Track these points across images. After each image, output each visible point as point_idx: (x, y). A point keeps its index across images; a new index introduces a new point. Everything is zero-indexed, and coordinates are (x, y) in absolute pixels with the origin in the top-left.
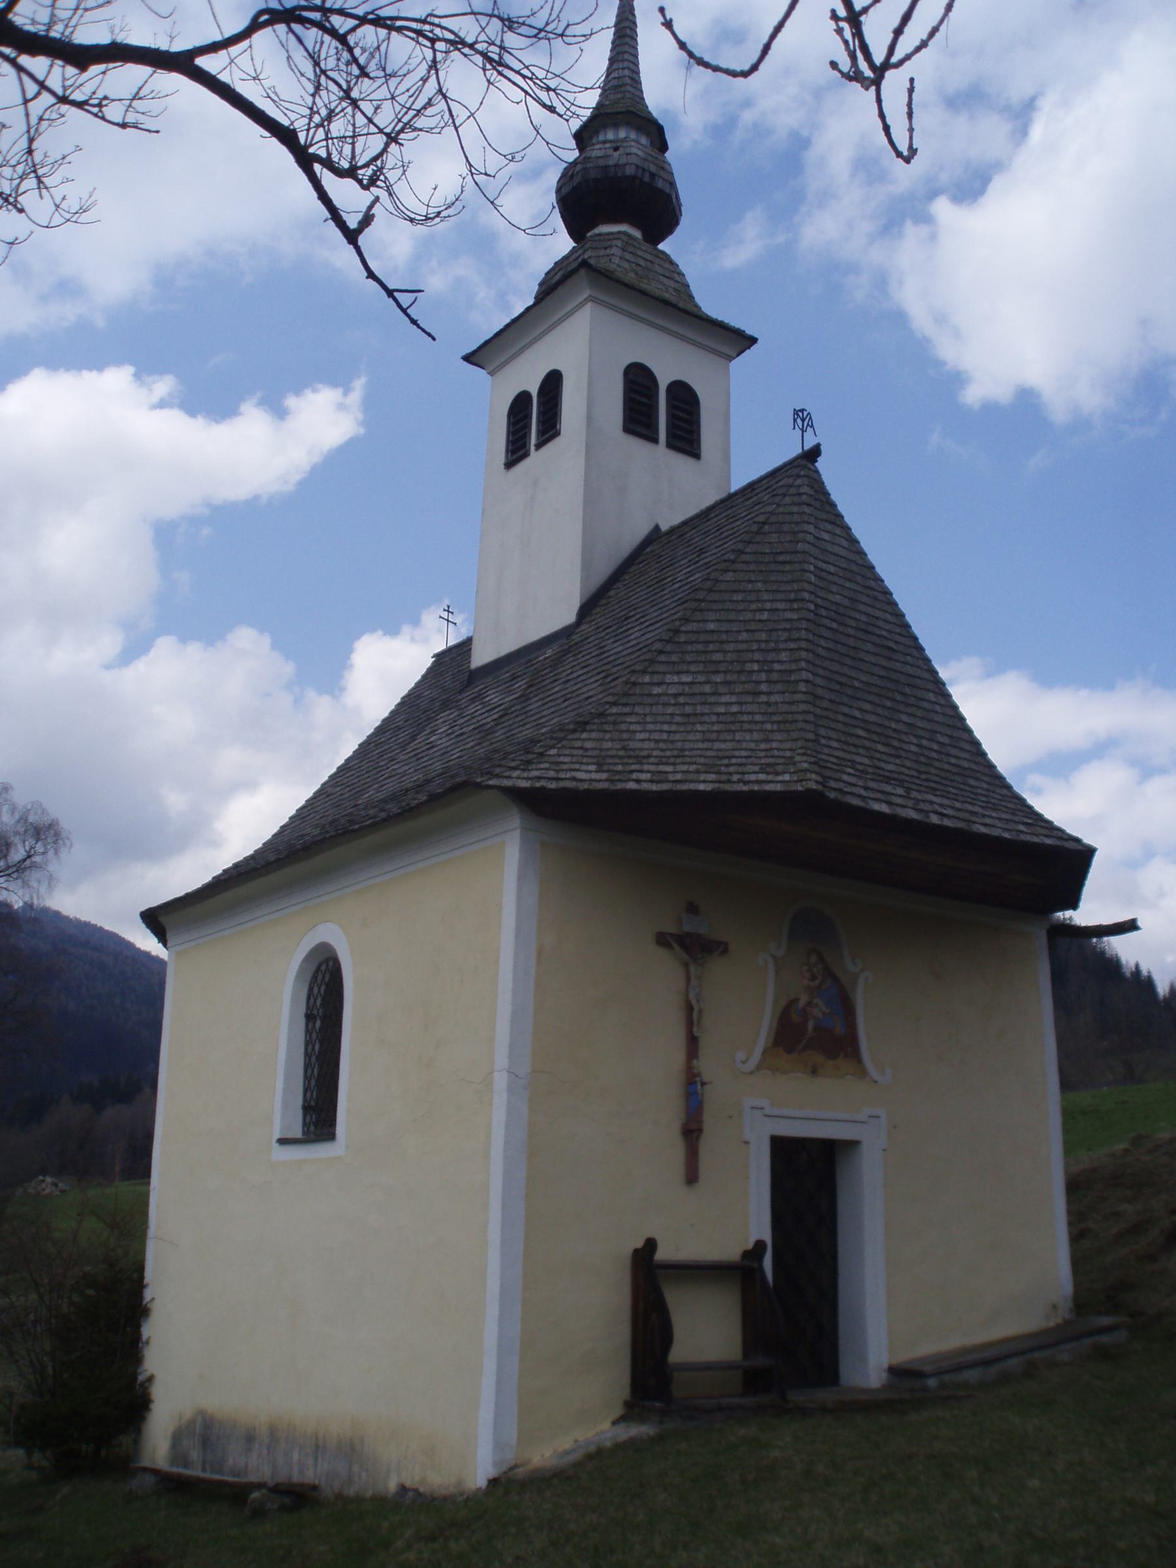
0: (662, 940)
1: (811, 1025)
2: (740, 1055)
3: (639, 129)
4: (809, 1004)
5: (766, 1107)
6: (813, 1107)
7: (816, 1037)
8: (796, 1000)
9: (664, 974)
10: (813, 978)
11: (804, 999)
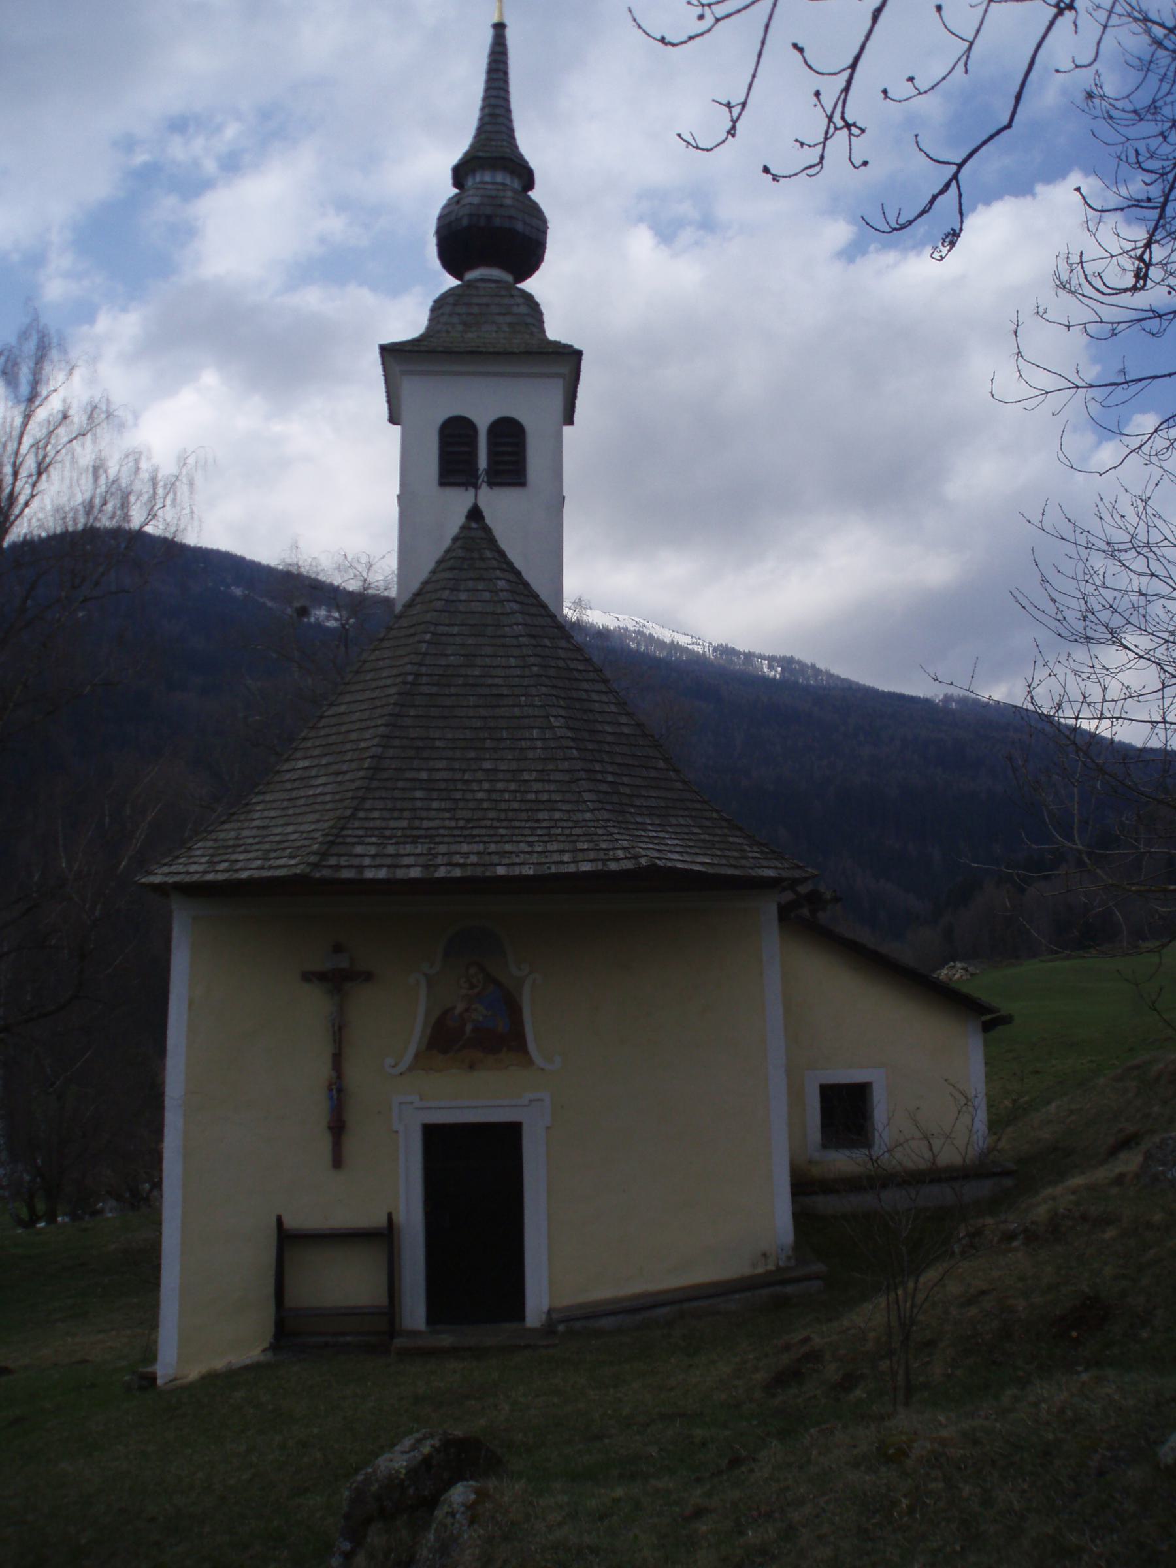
0: (307, 977)
1: (469, 1028)
2: (389, 1061)
3: (512, 173)
4: (467, 1010)
5: (413, 1099)
6: (472, 1097)
7: (481, 1033)
8: (454, 1008)
9: (314, 1005)
10: (472, 986)
11: (460, 1007)
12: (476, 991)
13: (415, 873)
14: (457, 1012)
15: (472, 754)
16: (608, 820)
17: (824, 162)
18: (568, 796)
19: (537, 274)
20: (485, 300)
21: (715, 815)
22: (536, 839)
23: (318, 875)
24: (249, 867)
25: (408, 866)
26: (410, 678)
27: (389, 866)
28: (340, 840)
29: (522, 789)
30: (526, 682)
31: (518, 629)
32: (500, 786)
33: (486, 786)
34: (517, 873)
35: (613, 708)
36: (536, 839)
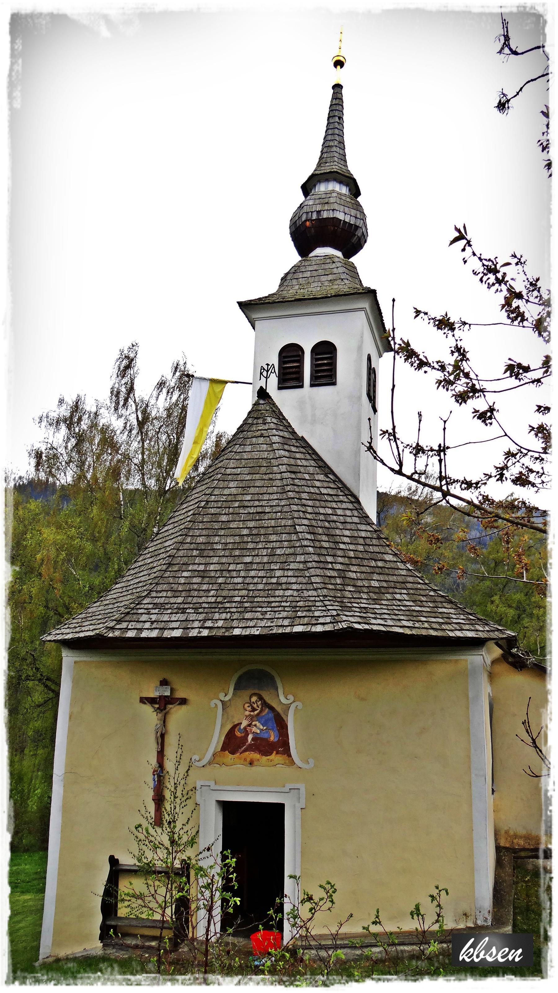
1: (250, 737)
4: (249, 725)
10: (254, 710)
11: (245, 723)
12: (256, 712)
13: (177, 633)
14: (242, 726)
15: (237, 553)
16: (326, 596)
17: (513, 56)
18: (300, 580)
19: (361, 252)
20: (315, 267)
21: (432, 593)
22: (270, 609)
23: (111, 635)
24: (88, 631)
25: (173, 629)
26: (203, 504)
27: (160, 629)
28: (135, 611)
29: (268, 575)
30: (283, 503)
31: (283, 468)
32: (252, 573)
33: (242, 574)
34: (247, 633)
35: (356, 520)
36: (270, 609)
